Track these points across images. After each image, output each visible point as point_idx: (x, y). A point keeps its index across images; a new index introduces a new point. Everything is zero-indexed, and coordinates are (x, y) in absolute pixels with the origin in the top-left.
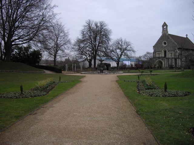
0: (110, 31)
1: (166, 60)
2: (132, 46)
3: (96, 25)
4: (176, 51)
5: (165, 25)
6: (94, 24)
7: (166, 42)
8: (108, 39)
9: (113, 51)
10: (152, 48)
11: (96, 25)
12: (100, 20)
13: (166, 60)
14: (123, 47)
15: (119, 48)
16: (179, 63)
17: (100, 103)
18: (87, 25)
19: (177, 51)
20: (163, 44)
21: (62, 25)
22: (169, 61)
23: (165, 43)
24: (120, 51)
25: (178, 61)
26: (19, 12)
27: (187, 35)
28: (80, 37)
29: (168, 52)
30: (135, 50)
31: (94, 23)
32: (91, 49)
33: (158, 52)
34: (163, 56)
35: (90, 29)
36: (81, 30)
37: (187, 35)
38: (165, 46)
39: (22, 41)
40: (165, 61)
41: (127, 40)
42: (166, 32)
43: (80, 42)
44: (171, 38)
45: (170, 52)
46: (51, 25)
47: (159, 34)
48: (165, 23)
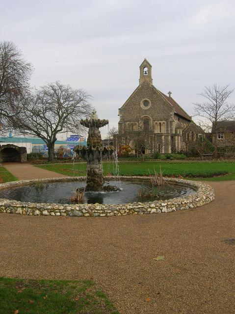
2: (88, 101)
4: (170, 120)
5: (146, 65)
7: (145, 99)
10: (117, 112)
14: (63, 103)
15: (51, 212)
16: (178, 145)
20: (142, 106)
22: (161, 140)
23: (146, 103)
24: (51, 112)
25: (177, 141)
27: (170, 93)
37: (170, 93)
38: (146, 108)
42: (147, 79)
45: (158, 122)
46: (63, 131)
47: (134, 84)
48: (145, 60)
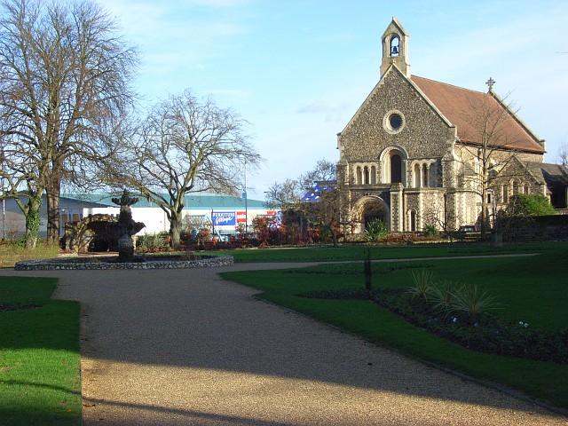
0: (128, 57)
2: (245, 131)
8: (121, 99)
11: (57, 19)
20: (387, 125)
23: (395, 121)
25: (457, 205)
27: (491, 82)
30: (257, 145)
34: (386, 178)
37: (491, 82)
41: (222, 105)
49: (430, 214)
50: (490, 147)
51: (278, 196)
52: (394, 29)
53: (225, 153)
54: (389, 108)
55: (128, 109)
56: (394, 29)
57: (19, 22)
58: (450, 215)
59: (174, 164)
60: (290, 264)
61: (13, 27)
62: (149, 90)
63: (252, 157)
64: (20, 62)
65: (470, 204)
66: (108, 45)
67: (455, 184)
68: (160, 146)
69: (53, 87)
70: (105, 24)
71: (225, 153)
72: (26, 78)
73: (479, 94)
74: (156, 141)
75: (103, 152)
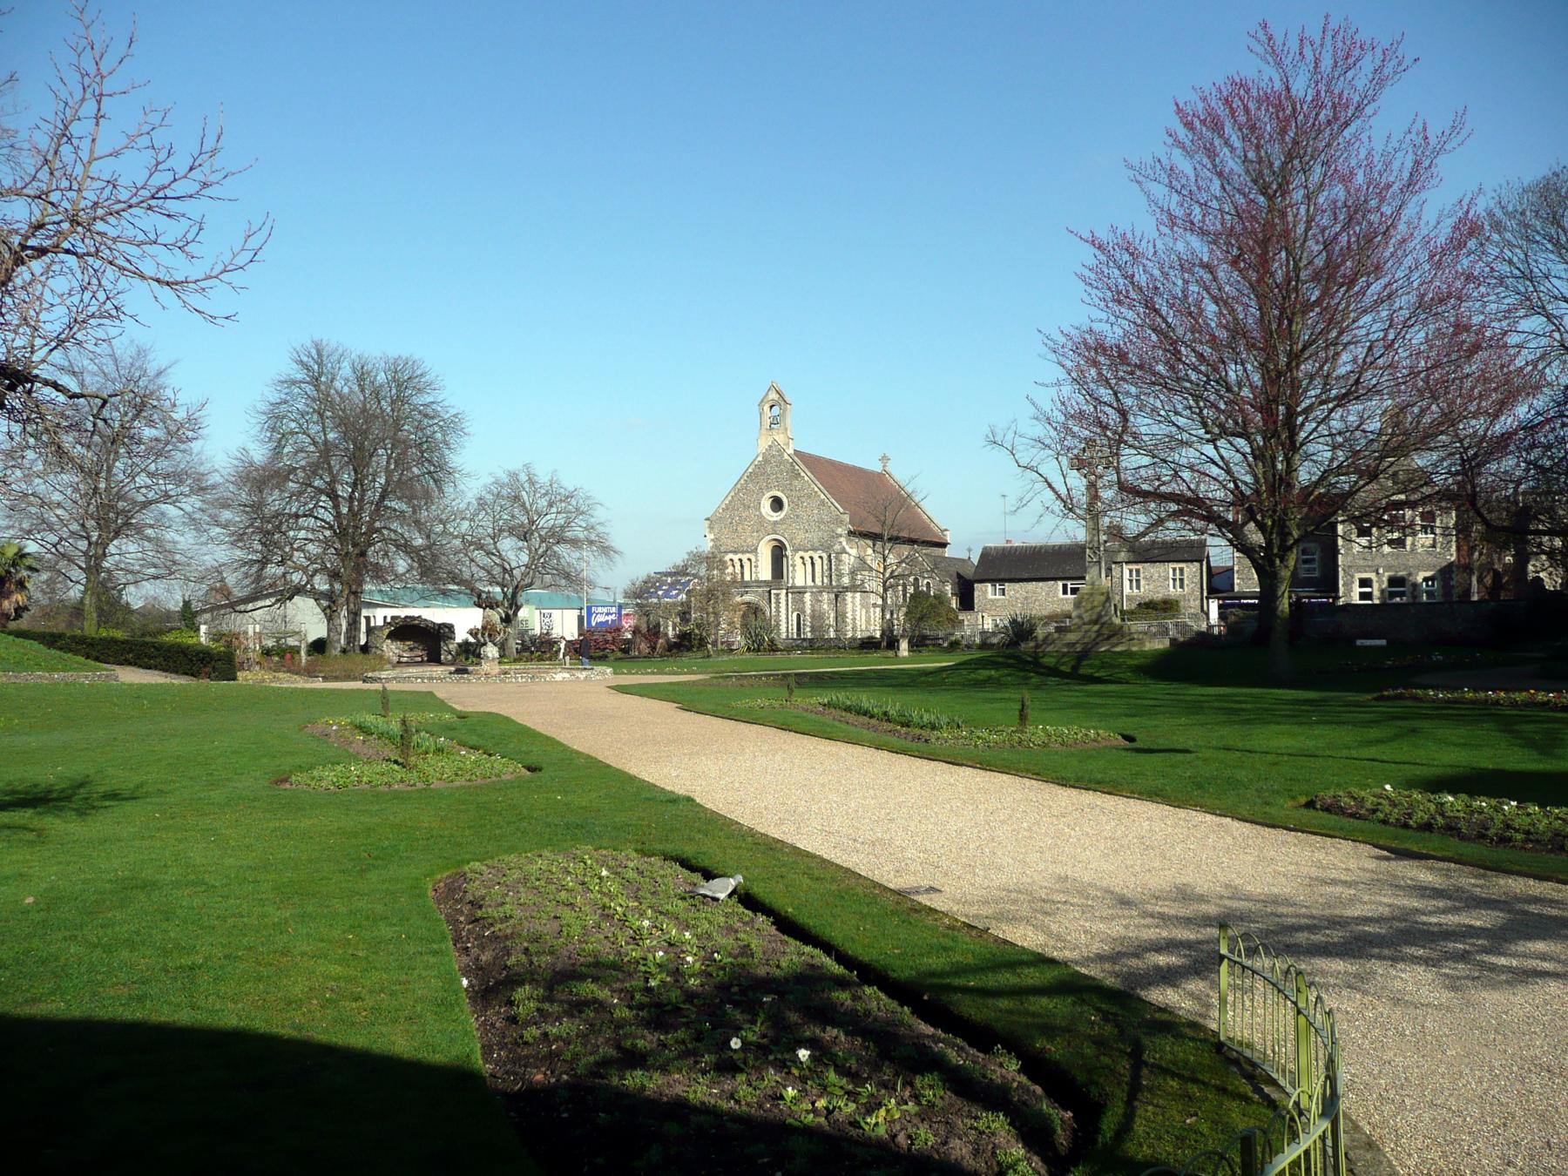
0: (453, 425)
1: (783, 596)
2: (599, 514)
3: (362, 376)
4: (837, 547)
6: (346, 370)
8: (439, 472)
9: (481, 547)
11: (362, 376)
12: (393, 352)
13: (783, 596)
17: (902, 798)
18: (300, 375)
19: (844, 551)
20: (766, 505)
21: (152, 369)
23: (777, 504)
25: (849, 606)
26: (1234, 138)
27: (884, 459)
28: (259, 454)
29: (797, 550)
30: (615, 541)
31: (346, 365)
32: (327, 533)
33: (735, 552)
34: (765, 573)
35: (324, 401)
36: (264, 407)
37: (884, 459)
39: (1201, 356)
40: (783, 605)
41: (568, 482)
43: (260, 479)
44: (807, 475)
49: (817, 617)
50: (890, 540)
51: (641, 592)
52: (773, 396)
53: (575, 543)
54: (769, 489)
55: (448, 489)
56: (773, 396)
57: (315, 381)
58: (840, 617)
59: (511, 555)
60: (670, 772)
61: (309, 388)
62: (477, 466)
63: (606, 550)
64: (314, 429)
65: (864, 605)
66: (429, 410)
67: (846, 581)
68: (75, 527)
69: (359, 460)
70: (421, 386)
71: (575, 543)
72: (326, 450)
73: (872, 473)
74: (486, 523)
75: (419, 542)
